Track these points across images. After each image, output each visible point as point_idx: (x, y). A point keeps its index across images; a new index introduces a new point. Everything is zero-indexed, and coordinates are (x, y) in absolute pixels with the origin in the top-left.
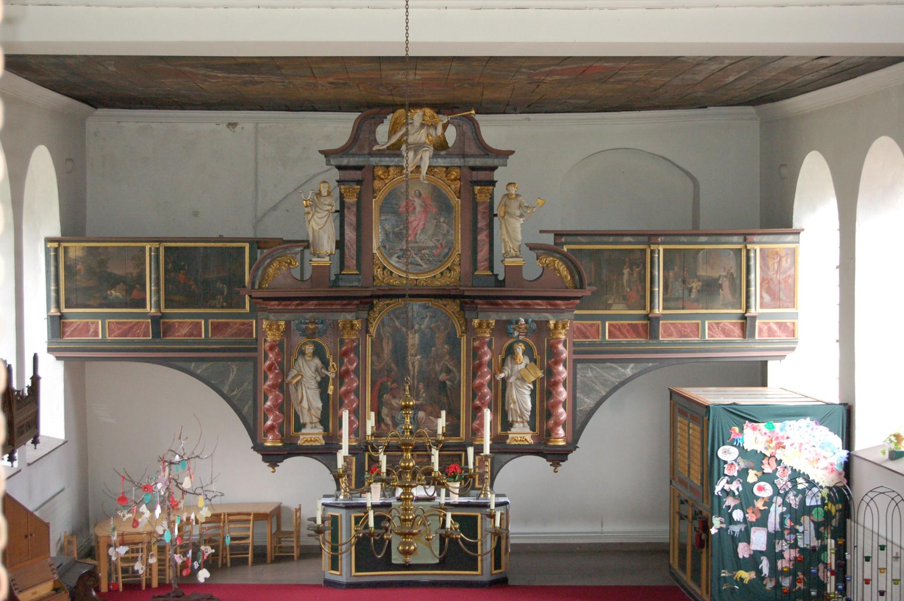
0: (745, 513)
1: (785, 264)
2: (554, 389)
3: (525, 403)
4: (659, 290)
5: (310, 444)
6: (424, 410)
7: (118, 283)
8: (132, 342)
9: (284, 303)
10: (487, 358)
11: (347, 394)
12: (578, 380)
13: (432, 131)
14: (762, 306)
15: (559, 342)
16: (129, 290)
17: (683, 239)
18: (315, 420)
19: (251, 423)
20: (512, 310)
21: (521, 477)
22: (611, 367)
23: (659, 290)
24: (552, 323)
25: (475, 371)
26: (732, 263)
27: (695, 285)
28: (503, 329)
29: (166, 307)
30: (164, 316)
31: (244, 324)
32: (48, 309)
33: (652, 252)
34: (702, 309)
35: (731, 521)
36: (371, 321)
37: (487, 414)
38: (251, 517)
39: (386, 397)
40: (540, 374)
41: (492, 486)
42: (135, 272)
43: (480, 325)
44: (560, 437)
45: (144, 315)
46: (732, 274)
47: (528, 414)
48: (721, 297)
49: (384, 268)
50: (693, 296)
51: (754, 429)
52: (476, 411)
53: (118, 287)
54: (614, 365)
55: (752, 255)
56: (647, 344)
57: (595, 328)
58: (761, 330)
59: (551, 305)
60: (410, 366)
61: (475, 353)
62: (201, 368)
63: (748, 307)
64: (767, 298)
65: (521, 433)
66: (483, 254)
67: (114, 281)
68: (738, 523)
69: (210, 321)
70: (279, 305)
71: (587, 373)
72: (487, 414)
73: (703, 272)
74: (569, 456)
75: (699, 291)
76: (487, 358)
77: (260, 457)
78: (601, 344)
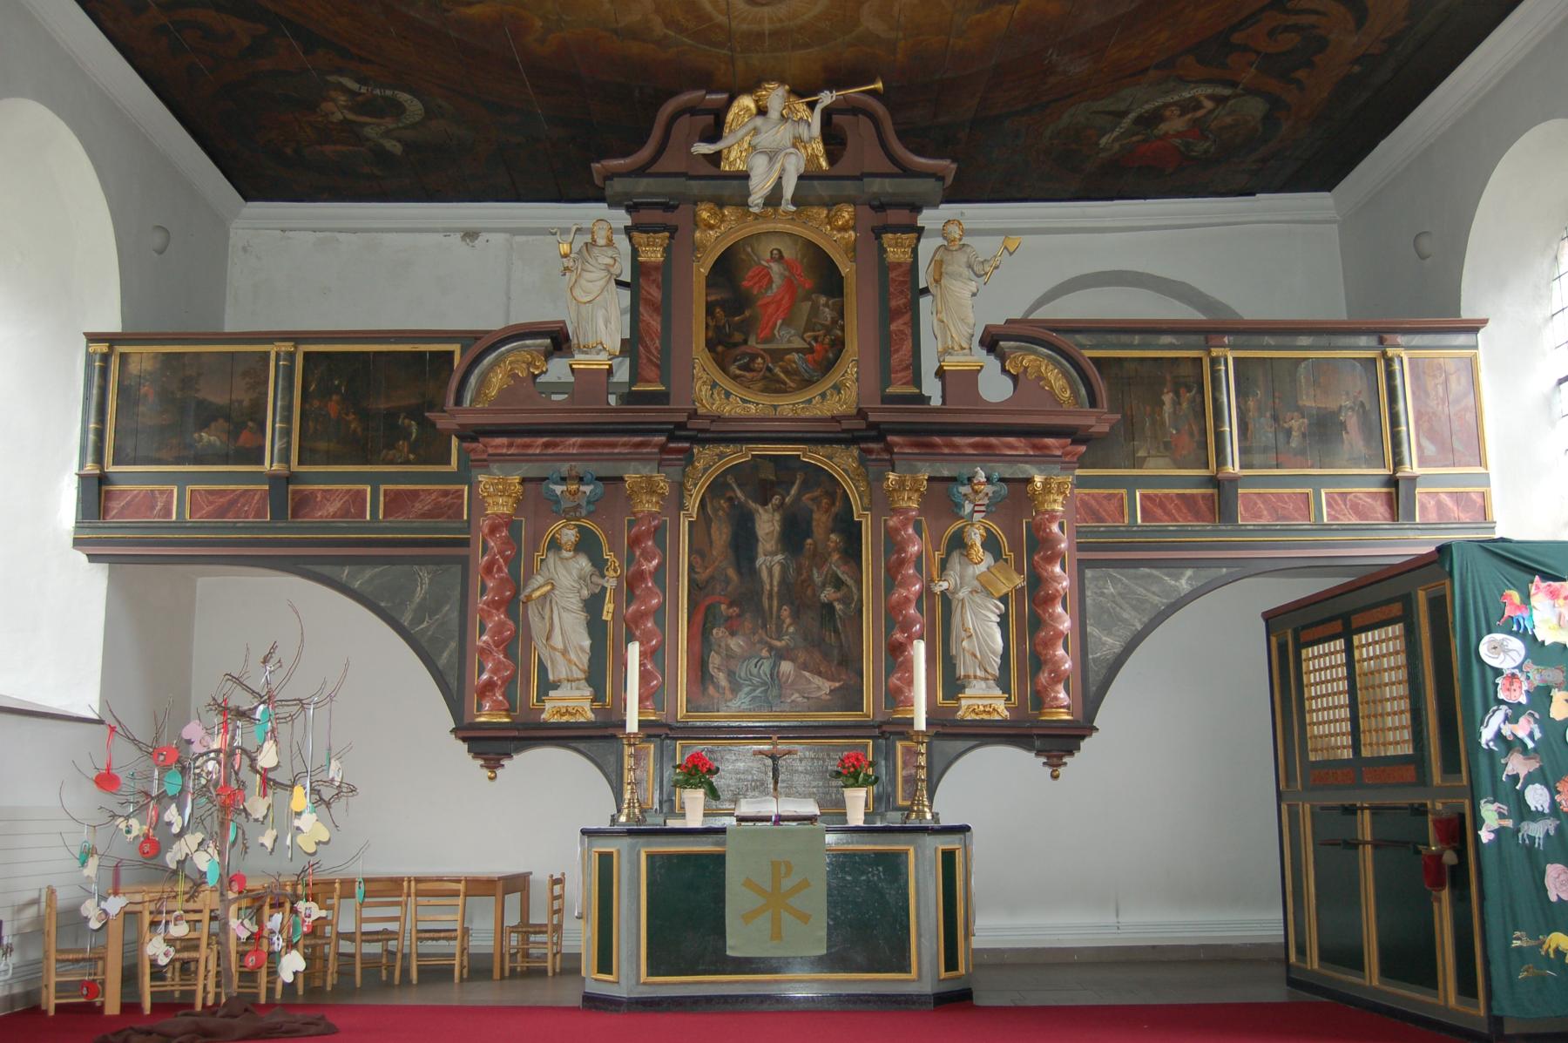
0: (1553, 791)
1: (1458, 385)
2: (1045, 611)
3: (991, 637)
4: (1231, 429)
5: (564, 719)
6: (793, 660)
7: (214, 419)
8: (234, 528)
9: (519, 441)
10: (914, 549)
11: (639, 617)
12: (1089, 601)
14: (1422, 463)
15: (1053, 518)
16: (235, 431)
17: (1268, 340)
19: (454, 684)
20: (958, 455)
21: (985, 791)
22: (1149, 576)
23: (1231, 429)
25: (892, 575)
27: (1297, 424)
28: (942, 498)
29: (300, 463)
30: (291, 478)
31: (446, 493)
32: (82, 465)
33: (1214, 361)
34: (1312, 467)
35: (1523, 812)
36: (689, 485)
37: (919, 650)
38: (461, 887)
39: (717, 633)
41: (931, 799)
42: (246, 399)
43: (901, 483)
44: (1062, 704)
46: (1362, 405)
48: (1346, 446)
49: (714, 385)
50: (1293, 445)
51: (1554, 595)
52: (896, 653)
53: (213, 425)
54: (1155, 572)
55: (1397, 367)
56: (1215, 532)
57: (1115, 501)
58: (1423, 507)
59: (1034, 447)
60: (765, 574)
61: (893, 544)
62: (361, 578)
63: (1398, 462)
64: (1430, 449)
65: (984, 699)
68: (1537, 816)
69: (382, 488)
70: (510, 446)
71: (1106, 587)
72: (919, 650)
74: (1082, 744)
75: (1304, 435)
76: (914, 549)
77: (465, 746)
78: (1128, 532)
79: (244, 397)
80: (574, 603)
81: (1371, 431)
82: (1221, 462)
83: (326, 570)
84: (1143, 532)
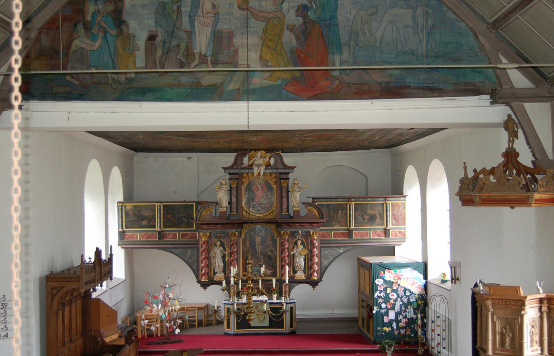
0: (386, 305)
1: (401, 208)
4: (353, 219)
8: (151, 241)
13: (265, 159)
14: (392, 225)
17: (361, 199)
18: (221, 271)
20: (296, 227)
21: (300, 293)
23: (353, 219)
24: (311, 232)
26: (381, 209)
27: (367, 217)
28: (293, 235)
30: (163, 231)
32: (119, 229)
33: (350, 205)
35: (381, 308)
37: (287, 268)
40: (307, 252)
42: (152, 215)
43: (284, 233)
44: (315, 276)
45: (155, 231)
47: (303, 268)
51: (389, 272)
56: (348, 240)
58: (392, 234)
61: (282, 244)
63: (387, 225)
64: (394, 222)
65: (300, 275)
66: (285, 206)
67: (143, 218)
68: (383, 309)
71: (325, 252)
72: (287, 268)
73: (370, 212)
78: (330, 240)
79: (150, 213)
80: (220, 257)
81: (382, 218)
82: (350, 226)
83: (170, 250)
84: (334, 240)
